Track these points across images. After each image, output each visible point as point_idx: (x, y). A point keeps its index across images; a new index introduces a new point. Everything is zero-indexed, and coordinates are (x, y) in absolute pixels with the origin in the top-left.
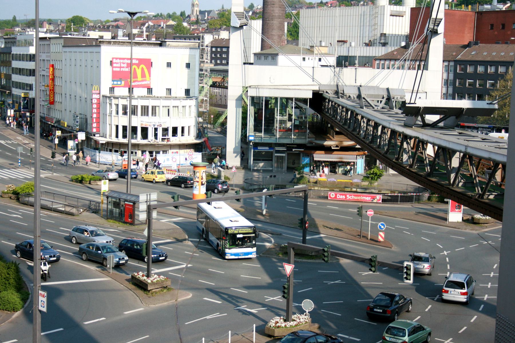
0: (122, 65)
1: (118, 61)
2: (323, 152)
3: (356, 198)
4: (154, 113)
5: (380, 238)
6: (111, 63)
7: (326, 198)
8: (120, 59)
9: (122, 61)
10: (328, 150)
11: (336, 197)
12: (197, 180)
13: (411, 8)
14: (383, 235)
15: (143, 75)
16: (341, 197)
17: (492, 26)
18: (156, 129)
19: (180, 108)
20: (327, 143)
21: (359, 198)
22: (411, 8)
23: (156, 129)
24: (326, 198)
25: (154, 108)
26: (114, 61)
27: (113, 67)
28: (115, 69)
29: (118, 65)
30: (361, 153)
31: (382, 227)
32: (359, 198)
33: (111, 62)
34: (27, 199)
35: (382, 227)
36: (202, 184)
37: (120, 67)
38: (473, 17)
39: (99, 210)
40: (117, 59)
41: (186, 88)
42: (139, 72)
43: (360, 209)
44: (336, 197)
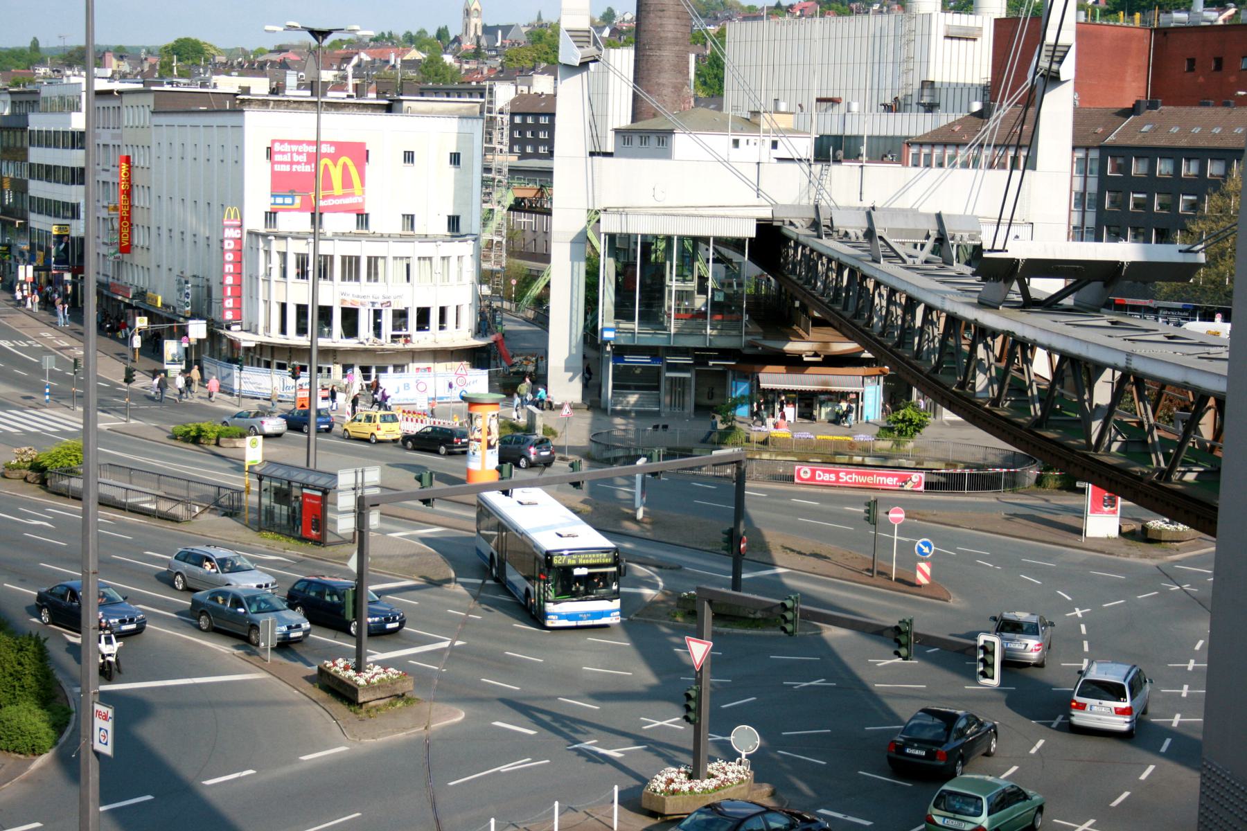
0: (296, 158)
1: (286, 148)
2: (782, 368)
3: (862, 479)
4: (373, 274)
5: (919, 576)
6: (270, 152)
7: (790, 479)
8: (291, 142)
9: (294, 148)
10: (795, 363)
11: (813, 478)
12: (477, 435)
13: (996, 20)
14: (928, 570)
15: (347, 182)
16: (827, 477)
17: (1192, 62)
18: (378, 314)
19: (437, 261)
20: (792, 347)
21: (869, 479)
22: (996, 20)
23: (378, 314)
24: (790, 479)
25: (373, 262)
26: (277, 147)
27: (273, 163)
28: (278, 168)
29: (287, 158)
30: (875, 370)
31: (926, 550)
32: (869, 479)
33: (269, 149)
34: (65, 482)
35: (926, 550)
36: (490, 447)
37: (292, 163)
38: (1145, 42)
39: (240, 508)
40: (282, 142)
42: (336, 174)
43: (872, 506)
44: (813, 478)
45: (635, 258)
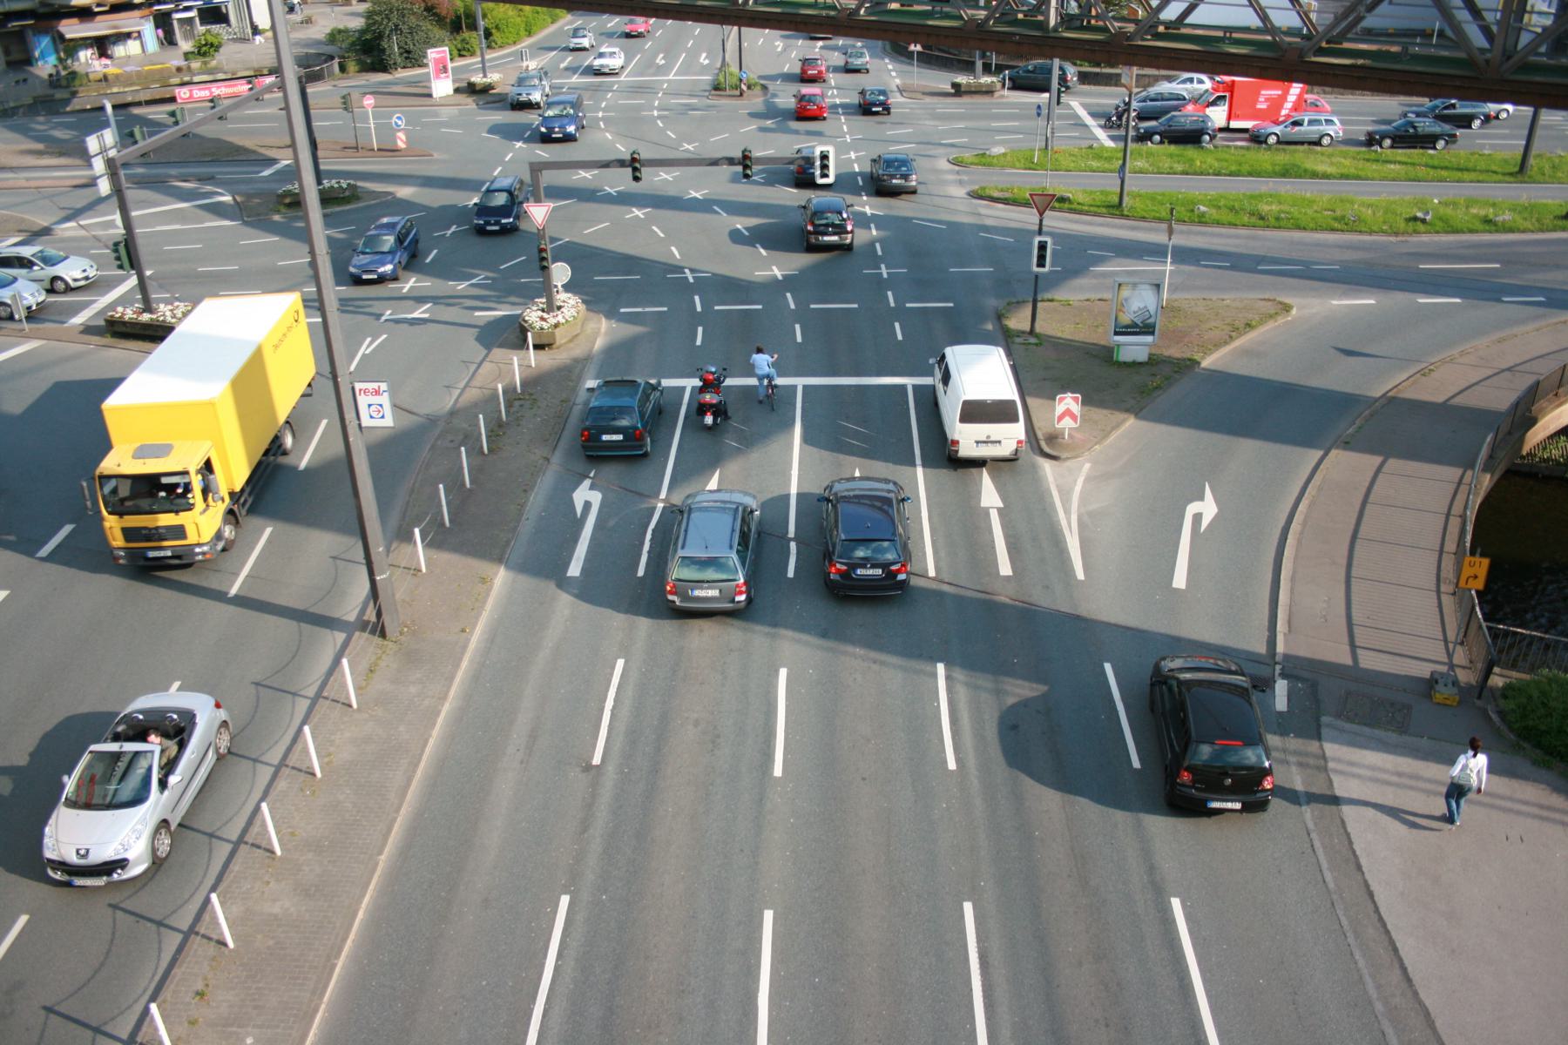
7: (173, 100)
24: (173, 100)
30: (146, 12)
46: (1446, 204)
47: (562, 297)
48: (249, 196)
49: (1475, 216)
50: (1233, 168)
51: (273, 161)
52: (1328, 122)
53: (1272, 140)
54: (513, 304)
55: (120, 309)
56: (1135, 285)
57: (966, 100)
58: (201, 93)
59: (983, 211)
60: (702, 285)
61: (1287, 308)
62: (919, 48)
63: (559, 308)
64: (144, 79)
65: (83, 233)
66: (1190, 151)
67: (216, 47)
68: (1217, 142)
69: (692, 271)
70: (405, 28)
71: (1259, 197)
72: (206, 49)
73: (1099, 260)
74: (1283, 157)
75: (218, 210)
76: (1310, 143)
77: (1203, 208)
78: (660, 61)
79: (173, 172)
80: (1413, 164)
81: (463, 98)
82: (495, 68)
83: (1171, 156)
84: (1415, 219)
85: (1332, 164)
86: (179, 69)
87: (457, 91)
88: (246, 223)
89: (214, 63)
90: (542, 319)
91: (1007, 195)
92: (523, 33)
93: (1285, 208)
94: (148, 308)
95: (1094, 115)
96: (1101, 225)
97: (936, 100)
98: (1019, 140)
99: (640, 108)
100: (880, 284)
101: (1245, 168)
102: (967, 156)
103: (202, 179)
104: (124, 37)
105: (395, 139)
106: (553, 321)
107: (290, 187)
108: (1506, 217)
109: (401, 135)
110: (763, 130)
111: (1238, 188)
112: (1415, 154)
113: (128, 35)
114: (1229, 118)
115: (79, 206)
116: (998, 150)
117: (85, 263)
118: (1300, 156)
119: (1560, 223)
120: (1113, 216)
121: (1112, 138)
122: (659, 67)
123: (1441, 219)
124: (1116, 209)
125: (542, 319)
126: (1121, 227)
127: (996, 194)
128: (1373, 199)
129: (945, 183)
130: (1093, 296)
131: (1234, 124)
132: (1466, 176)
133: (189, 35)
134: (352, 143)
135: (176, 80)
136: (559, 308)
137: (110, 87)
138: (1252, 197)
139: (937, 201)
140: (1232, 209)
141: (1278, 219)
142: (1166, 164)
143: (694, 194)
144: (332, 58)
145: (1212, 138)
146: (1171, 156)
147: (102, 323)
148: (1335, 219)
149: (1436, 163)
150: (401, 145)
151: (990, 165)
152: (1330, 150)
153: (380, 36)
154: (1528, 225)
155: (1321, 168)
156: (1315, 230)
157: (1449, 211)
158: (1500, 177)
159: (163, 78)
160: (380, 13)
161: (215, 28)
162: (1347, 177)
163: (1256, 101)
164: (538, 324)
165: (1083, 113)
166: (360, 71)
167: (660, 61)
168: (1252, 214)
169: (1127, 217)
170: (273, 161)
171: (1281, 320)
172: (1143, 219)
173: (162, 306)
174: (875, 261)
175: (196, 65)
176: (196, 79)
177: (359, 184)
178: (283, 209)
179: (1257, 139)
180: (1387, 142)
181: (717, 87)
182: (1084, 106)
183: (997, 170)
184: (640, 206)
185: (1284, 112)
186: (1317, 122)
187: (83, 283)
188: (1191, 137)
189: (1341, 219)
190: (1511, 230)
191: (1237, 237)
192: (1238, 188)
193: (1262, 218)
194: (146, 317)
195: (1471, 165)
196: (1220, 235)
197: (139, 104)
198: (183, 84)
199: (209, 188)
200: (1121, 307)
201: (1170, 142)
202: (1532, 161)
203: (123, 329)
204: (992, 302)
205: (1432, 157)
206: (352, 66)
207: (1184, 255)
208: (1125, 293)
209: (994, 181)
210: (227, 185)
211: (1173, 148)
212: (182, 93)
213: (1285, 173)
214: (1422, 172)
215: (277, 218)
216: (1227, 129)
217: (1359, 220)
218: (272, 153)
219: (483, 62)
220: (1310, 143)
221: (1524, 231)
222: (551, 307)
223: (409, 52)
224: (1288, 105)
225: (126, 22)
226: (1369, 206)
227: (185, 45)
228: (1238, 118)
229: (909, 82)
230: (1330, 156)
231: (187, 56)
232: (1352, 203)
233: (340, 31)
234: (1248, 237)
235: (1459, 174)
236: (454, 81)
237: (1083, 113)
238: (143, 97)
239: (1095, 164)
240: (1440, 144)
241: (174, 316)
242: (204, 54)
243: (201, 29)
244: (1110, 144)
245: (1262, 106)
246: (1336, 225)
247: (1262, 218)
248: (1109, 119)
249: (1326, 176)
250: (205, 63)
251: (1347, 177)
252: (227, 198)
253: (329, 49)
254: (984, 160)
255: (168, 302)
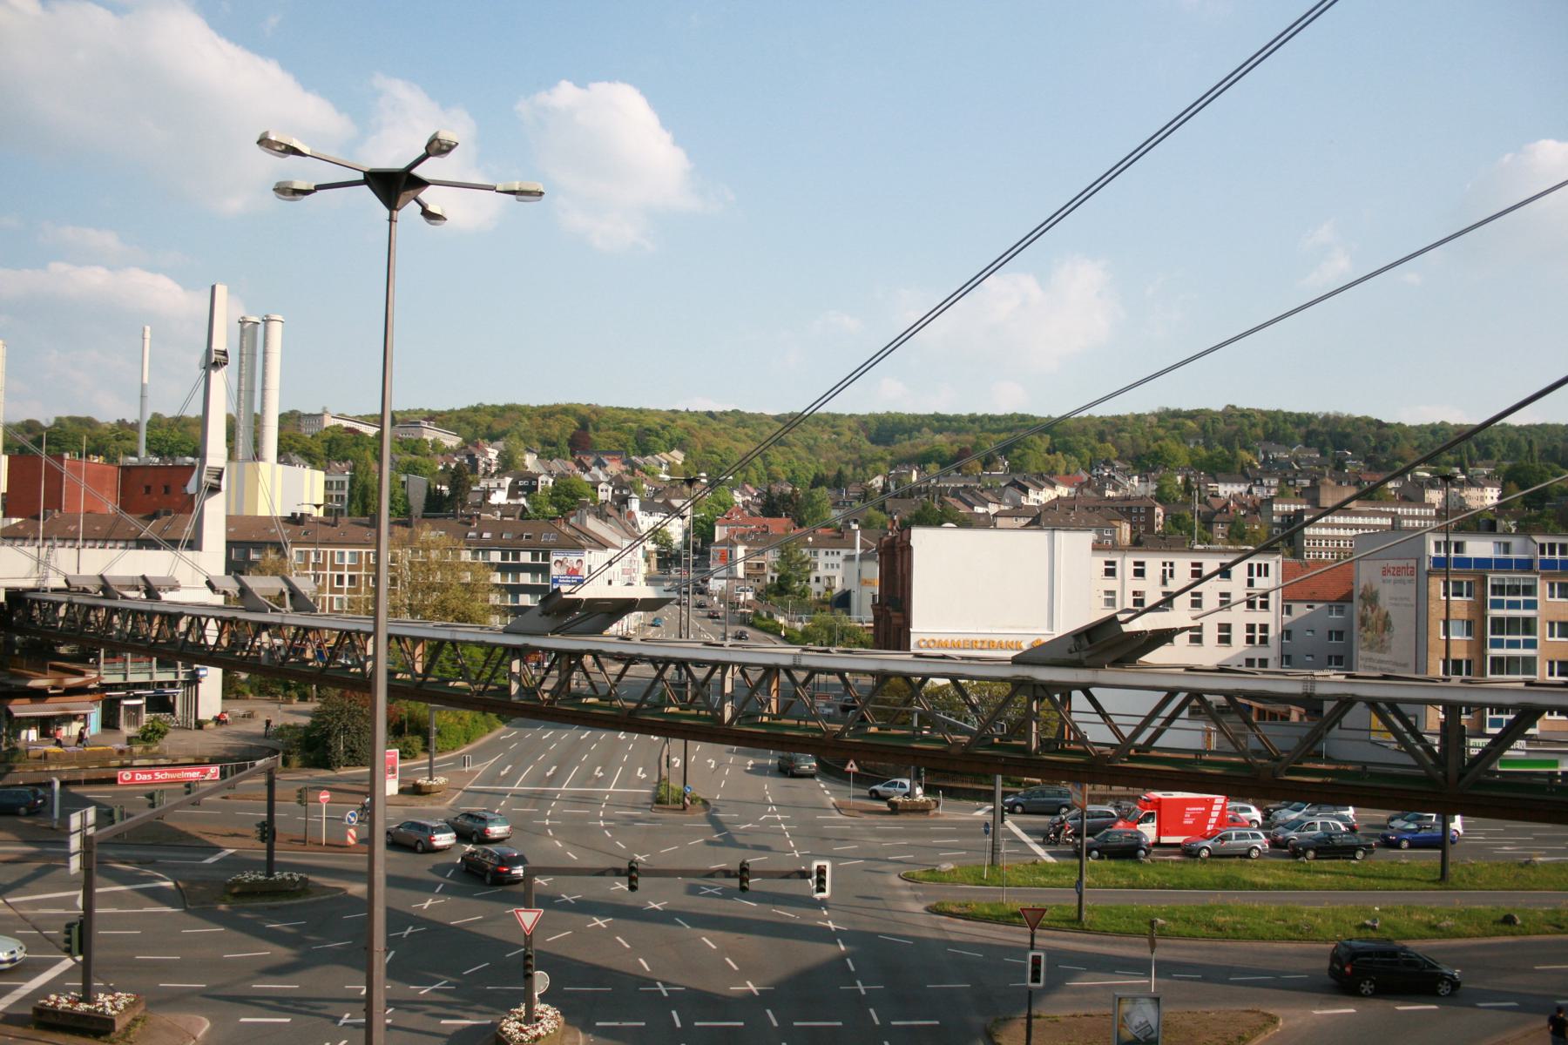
2: (27, 700)
3: (172, 776)
5: (350, 840)
7: (113, 781)
10: (39, 695)
11: (133, 779)
16: (145, 777)
17: (148, 489)
20: (33, 683)
21: (178, 775)
24: (113, 781)
30: (98, 696)
32: (178, 775)
34: (40, 864)
38: (113, 475)
39: (1138, 847)
41: (261, 464)
43: (151, 796)
44: (133, 779)
45: (1375, 527)
46: (1388, 911)
47: (539, 1007)
48: (192, 883)
49: (1420, 922)
50: (1176, 881)
51: (218, 849)
52: (1255, 836)
53: (1205, 853)
54: (480, 1012)
55: (53, 997)
56: (1134, 999)
57: (902, 818)
58: (142, 777)
59: (945, 926)
60: (676, 999)
61: (1273, 1020)
62: (855, 768)
63: (538, 1019)
64: (84, 760)
65: (9, 911)
66: (1130, 866)
67: (161, 734)
68: (1152, 856)
69: (665, 984)
70: (353, 729)
71: (1211, 909)
72: (150, 735)
73: (1072, 975)
74: (1219, 870)
75: (159, 896)
76: (1241, 856)
77: (1160, 921)
78: (598, 773)
79: (111, 853)
80: (1341, 874)
81: (405, 798)
82: (441, 772)
83: (1114, 870)
84: (1365, 926)
85: (1267, 876)
86: (121, 752)
87: (401, 791)
88: (187, 911)
89: (156, 749)
90: (521, 1030)
91: (965, 911)
92: (462, 740)
93: (1237, 918)
94: (87, 996)
95: (1028, 832)
96: (1065, 939)
97: (874, 818)
98: (963, 857)
99: (585, 817)
100: (862, 1002)
101: (1187, 881)
102: (917, 871)
103: (142, 863)
104: (69, 719)
105: (346, 834)
106: (534, 1033)
107: (239, 876)
108: (1448, 922)
109: (352, 831)
110: (709, 843)
111: (1187, 901)
112: (1339, 864)
113: (75, 718)
114: (1159, 834)
115: (8, 882)
116: (947, 866)
117: (14, 944)
118: (1233, 868)
119: (1501, 927)
120: (1074, 930)
121: (1051, 854)
122: (598, 779)
123: (1388, 925)
124: (1076, 923)
125: (521, 1030)
126: (1078, 940)
127: (955, 910)
128: (1317, 908)
129: (901, 898)
130: (1081, 1012)
131: (1164, 840)
132: (1393, 884)
133: (134, 721)
134: (300, 835)
135: (116, 763)
136: (538, 1019)
137: (47, 765)
138: (1204, 909)
139: (898, 916)
140: (1188, 921)
141: (1235, 930)
142: (1111, 878)
143: (654, 905)
144: (277, 752)
145: (1148, 853)
146: (1114, 870)
147: (30, 1012)
148: (1289, 928)
149: (1362, 871)
150: (351, 841)
151: (941, 881)
152: (1261, 862)
153: (328, 735)
154: (1470, 929)
155: (1259, 879)
156: (1273, 939)
157: (1391, 918)
158: (1424, 885)
159: (103, 759)
160: (332, 713)
161: (163, 716)
162: (1284, 887)
163: (1183, 818)
164: (518, 1036)
165: (1017, 830)
166: (303, 766)
167: (598, 773)
168: (1208, 925)
169: (1088, 931)
170: (218, 849)
171: (1271, 1032)
172: (1104, 932)
173: (101, 996)
174: (851, 978)
175: (138, 749)
176: (136, 763)
177: (311, 878)
178: (229, 899)
179: (1189, 853)
180: (1311, 854)
181: (659, 801)
182: (1016, 823)
183: (949, 886)
184: (602, 916)
185: (1209, 828)
186: (1245, 836)
187: (7, 966)
188: (1129, 851)
189: (1295, 928)
190: (1458, 936)
191: (1198, 948)
192: (1187, 901)
193: (1219, 929)
194: (83, 1007)
195: (1395, 874)
196: (1183, 947)
197: (78, 783)
198: (123, 767)
199: (149, 872)
200: (1123, 1023)
201: (1110, 858)
202: (1451, 869)
203: (53, 1020)
204: (978, 1020)
205: (1356, 866)
206: (295, 761)
207: (1165, 969)
208: (1126, 1007)
209: (951, 897)
210: (170, 871)
211: (1113, 863)
212: (126, 775)
213: (1227, 884)
214: (1352, 881)
215: (222, 907)
216: (1158, 844)
217: (1312, 928)
218: (216, 841)
219: (431, 764)
220: (1241, 856)
221: (1469, 936)
222: (530, 1018)
223: (353, 751)
224: (1213, 821)
225: (75, 705)
226: (1317, 915)
227: (127, 730)
228: (1167, 834)
229: (845, 800)
230: (1263, 868)
231: (130, 740)
232: (1300, 912)
233: (288, 727)
234: (1209, 948)
235: (1387, 883)
236: (400, 782)
237: (1017, 830)
238: (83, 776)
239: (1043, 879)
240: (1360, 855)
241: (114, 1008)
242: (148, 740)
243: (145, 717)
244: (1050, 859)
245: (1188, 822)
246: (1292, 934)
247: (1219, 929)
248: (1046, 836)
249: (1264, 887)
250: (147, 748)
251: (1284, 887)
252: (169, 884)
253: (271, 743)
254: (934, 875)
255: (111, 991)
